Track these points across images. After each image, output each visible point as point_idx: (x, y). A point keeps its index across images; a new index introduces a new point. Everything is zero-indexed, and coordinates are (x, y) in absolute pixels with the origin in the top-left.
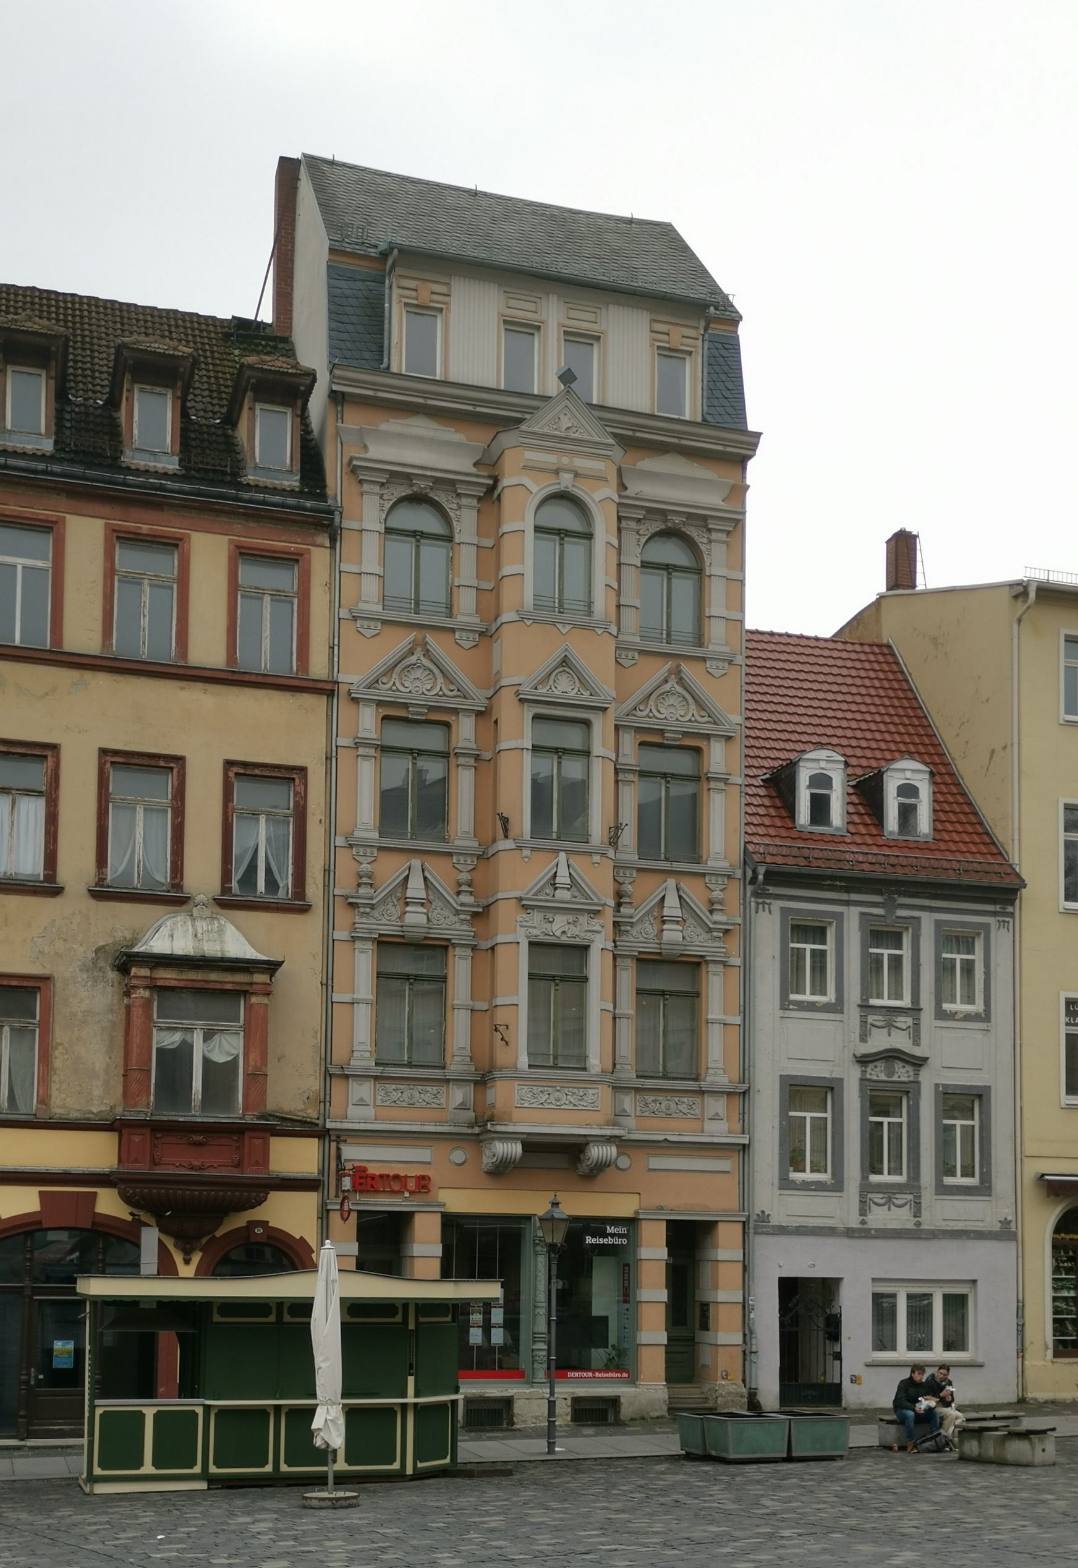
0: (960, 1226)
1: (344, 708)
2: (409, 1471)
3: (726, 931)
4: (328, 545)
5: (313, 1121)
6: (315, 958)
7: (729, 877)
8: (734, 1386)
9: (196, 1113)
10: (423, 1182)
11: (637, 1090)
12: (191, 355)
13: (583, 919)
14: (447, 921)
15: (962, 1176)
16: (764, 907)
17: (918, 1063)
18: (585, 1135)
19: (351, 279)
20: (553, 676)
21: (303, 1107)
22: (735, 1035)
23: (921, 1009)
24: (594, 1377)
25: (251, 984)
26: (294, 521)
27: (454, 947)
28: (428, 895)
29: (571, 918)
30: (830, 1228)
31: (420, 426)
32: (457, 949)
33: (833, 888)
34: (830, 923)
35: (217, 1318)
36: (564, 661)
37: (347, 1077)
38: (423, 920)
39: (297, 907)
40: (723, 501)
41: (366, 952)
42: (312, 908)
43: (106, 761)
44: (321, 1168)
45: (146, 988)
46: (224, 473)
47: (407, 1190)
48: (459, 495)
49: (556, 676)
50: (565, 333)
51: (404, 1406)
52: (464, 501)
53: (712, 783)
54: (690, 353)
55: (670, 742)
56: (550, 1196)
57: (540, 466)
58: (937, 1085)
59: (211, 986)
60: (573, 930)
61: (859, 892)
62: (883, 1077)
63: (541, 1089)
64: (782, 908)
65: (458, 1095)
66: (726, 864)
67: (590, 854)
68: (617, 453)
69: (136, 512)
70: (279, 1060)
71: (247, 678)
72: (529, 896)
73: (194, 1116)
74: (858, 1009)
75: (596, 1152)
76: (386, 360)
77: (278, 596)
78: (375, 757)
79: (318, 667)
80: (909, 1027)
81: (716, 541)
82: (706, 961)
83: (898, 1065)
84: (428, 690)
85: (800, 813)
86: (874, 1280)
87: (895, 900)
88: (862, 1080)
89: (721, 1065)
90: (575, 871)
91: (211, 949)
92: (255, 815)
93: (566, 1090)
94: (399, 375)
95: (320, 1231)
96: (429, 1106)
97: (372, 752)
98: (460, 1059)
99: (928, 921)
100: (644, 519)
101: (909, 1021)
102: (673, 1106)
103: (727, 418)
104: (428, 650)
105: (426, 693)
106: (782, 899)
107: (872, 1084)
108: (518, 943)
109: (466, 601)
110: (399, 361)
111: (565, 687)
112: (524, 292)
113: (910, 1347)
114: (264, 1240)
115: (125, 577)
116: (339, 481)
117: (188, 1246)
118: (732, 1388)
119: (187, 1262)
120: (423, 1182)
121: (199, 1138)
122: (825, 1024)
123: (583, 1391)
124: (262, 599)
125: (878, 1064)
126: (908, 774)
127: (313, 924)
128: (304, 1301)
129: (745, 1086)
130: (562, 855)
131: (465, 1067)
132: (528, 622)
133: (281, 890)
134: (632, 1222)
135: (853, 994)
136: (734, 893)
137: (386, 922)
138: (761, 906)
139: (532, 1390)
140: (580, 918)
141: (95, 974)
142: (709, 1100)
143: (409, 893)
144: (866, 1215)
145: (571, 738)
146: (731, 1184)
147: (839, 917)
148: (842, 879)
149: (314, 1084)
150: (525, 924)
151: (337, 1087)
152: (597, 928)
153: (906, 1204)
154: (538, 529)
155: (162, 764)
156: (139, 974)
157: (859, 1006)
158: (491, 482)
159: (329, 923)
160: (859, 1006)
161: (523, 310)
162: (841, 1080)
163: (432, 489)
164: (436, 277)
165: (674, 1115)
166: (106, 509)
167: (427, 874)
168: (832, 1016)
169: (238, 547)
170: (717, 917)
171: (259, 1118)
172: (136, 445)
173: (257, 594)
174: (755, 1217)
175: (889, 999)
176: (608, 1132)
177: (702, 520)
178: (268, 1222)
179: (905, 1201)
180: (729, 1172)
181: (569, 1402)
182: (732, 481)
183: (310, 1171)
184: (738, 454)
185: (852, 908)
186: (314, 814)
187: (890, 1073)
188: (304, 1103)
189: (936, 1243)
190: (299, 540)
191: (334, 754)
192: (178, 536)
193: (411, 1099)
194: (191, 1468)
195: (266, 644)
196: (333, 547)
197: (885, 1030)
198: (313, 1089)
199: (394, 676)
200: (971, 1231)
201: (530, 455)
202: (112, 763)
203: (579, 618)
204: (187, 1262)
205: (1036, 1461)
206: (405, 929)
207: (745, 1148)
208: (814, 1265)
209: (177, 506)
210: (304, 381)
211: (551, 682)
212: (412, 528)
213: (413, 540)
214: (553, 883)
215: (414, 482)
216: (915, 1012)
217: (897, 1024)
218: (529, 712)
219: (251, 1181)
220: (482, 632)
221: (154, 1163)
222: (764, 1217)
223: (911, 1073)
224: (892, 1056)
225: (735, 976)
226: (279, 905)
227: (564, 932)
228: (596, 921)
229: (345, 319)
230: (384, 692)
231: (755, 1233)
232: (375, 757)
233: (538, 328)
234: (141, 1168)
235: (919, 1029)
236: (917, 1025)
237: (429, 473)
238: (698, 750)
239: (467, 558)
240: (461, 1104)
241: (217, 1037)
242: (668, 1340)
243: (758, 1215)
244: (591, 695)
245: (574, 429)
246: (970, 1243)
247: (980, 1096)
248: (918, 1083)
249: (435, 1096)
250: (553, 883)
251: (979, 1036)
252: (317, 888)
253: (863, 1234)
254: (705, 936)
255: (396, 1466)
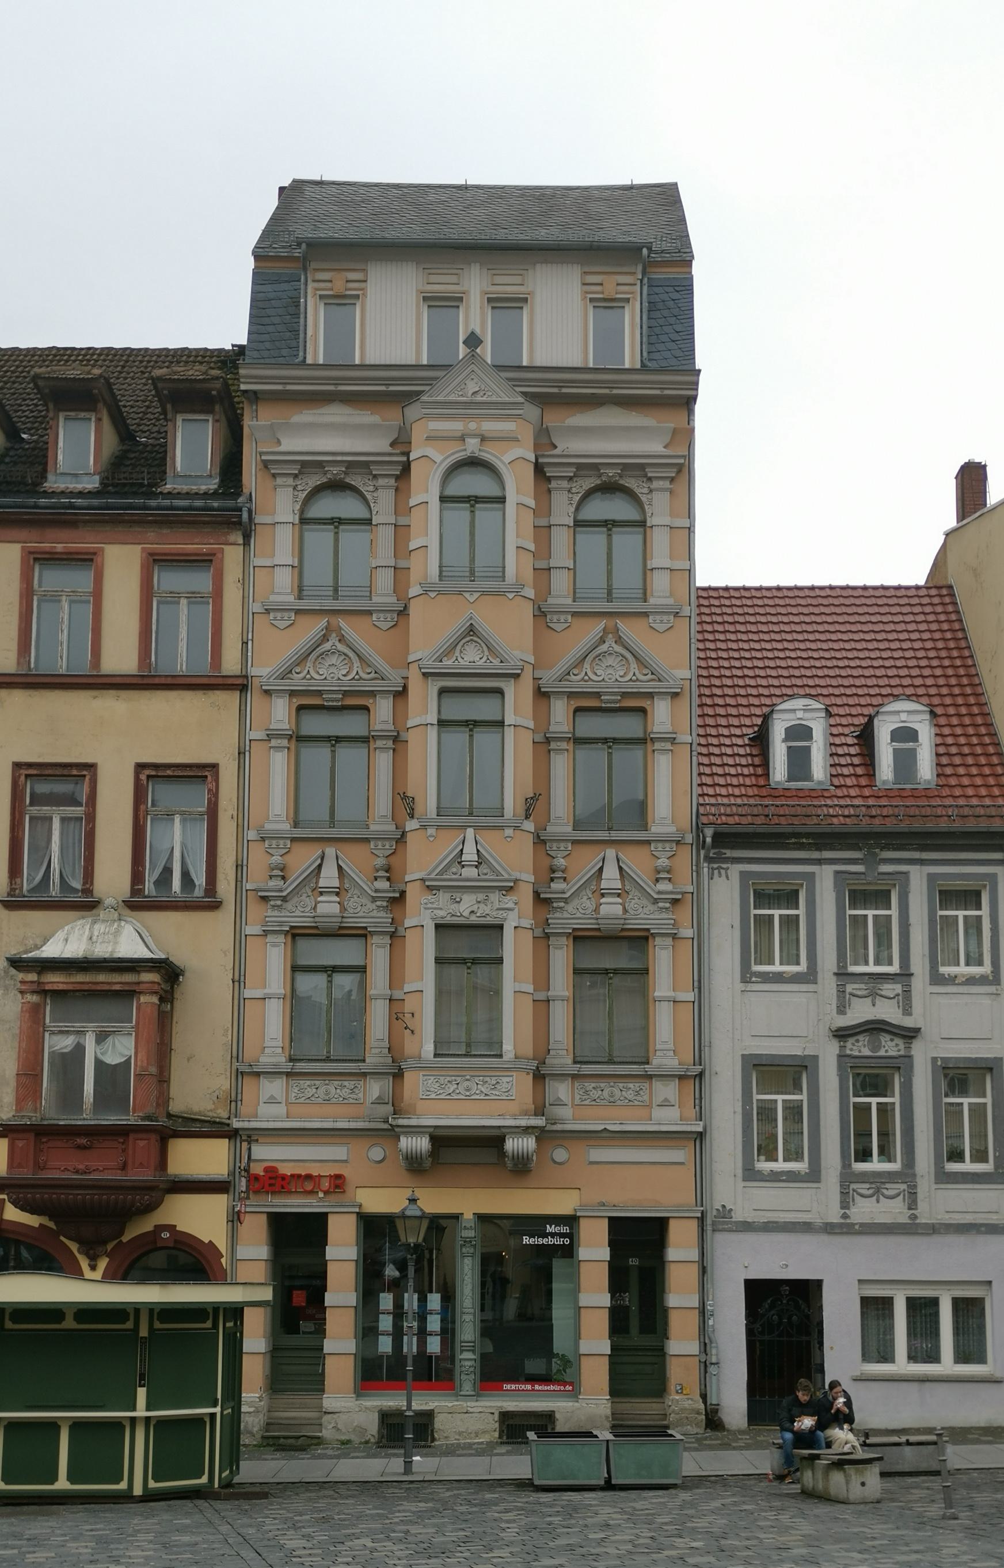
0: (968, 1219)
1: (255, 699)
2: (138, 1491)
3: (675, 902)
4: (241, 541)
5: (224, 1120)
6: (226, 955)
7: (678, 842)
8: (690, 1402)
9: (87, 1117)
10: (338, 1182)
11: (574, 1077)
12: (101, 376)
13: (495, 897)
14: (646, 910)
15: (972, 1161)
16: (720, 873)
17: (910, 1035)
18: (499, 1127)
19: (278, 282)
20: (459, 647)
21: (213, 1106)
22: (686, 1014)
23: (912, 974)
24: (533, 1390)
25: (139, 983)
26: (205, 523)
27: (372, 935)
28: (623, 885)
29: (481, 897)
30: (805, 1223)
31: (336, 414)
32: (374, 937)
33: (801, 847)
34: (985, 886)
35: (9, 1325)
36: (471, 630)
37: (258, 1074)
38: (618, 910)
39: (206, 904)
40: (665, 447)
41: (278, 946)
42: (224, 903)
43: (20, 775)
44: (232, 1168)
45: (33, 992)
46: (142, 485)
47: (322, 1191)
48: (650, 479)
49: (463, 646)
50: (489, 300)
51: (133, 1420)
52: (381, 482)
53: (656, 744)
54: (628, 300)
55: (609, 705)
56: (408, 1193)
57: (445, 435)
58: (934, 1060)
59: (99, 988)
60: (483, 909)
61: (832, 848)
62: (866, 1052)
63: (449, 1079)
64: (741, 873)
65: (375, 1088)
66: (673, 829)
67: (501, 828)
68: (532, 412)
69: (51, 533)
70: (188, 1060)
71: (157, 681)
72: (433, 876)
73: (84, 1119)
74: (834, 978)
75: (512, 1145)
76: (301, 354)
77: (194, 598)
78: (567, 750)
79: (231, 664)
80: (898, 995)
81: (657, 490)
82: (652, 934)
83: (885, 1039)
84: (621, 677)
85: (775, 769)
86: (860, 1281)
87: (875, 855)
88: (840, 1056)
89: (672, 1046)
90: (484, 848)
91: (102, 951)
92: (170, 815)
93: (477, 1079)
94: (316, 366)
95: (230, 1234)
96: (631, 1103)
97: (285, 742)
98: (377, 1051)
99: (918, 878)
100: (574, 476)
101: (898, 988)
102: (617, 1092)
103: (674, 362)
104: (620, 637)
105: (619, 679)
106: (742, 863)
107: (853, 1060)
108: (423, 926)
109: (384, 581)
110: (317, 352)
111: (471, 657)
112: (446, 266)
113: (912, 1358)
114: (171, 1245)
115: (44, 595)
116: (254, 478)
117: (92, 1252)
118: (687, 1404)
119: (93, 1268)
120: (338, 1182)
121: (83, 1141)
122: (796, 997)
123: (512, 1405)
124: (179, 603)
125: (861, 1037)
126: (903, 716)
127: (220, 923)
128: (201, 1306)
129: (699, 1068)
130: (470, 832)
131: (382, 1060)
132: (433, 595)
133: (197, 888)
134: (571, 1220)
135: (828, 961)
136: (684, 859)
137: (298, 914)
138: (716, 872)
139: (456, 1403)
140: (491, 896)
141: (7, 982)
142: (657, 1085)
143: (604, 884)
144: (849, 1209)
145: (482, 709)
146: (686, 1176)
147: (811, 877)
148: (808, 835)
149: (223, 1083)
150: (430, 905)
151: (248, 1083)
152: (510, 905)
153: (898, 1195)
154: (443, 499)
155: (75, 772)
156: (26, 980)
157: (835, 974)
158: (404, 459)
159: (240, 918)
160: (835, 974)
161: (443, 284)
162: (815, 1058)
163: (621, 477)
164: (352, 266)
165: (619, 1103)
166: (23, 533)
167: (340, 863)
168: (804, 987)
169: (151, 554)
170: (663, 886)
171: (143, 1119)
172: (60, 470)
173: (174, 598)
174: (715, 1213)
175: (781, 964)
176: (523, 1122)
177: (639, 469)
178: (175, 1226)
179: (898, 1191)
180: (682, 1163)
181: (496, 1417)
182: (672, 425)
183: (220, 1173)
184: (681, 397)
185: (824, 867)
186: (225, 810)
187: (876, 1047)
188: (214, 1103)
189: (936, 1239)
190: (212, 541)
191: (247, 748)
192: (92, 551)
193: (327, 1095)
194: (118, 1483)
195: (183, 646)
196: (246, 543)
197: (869, 1000)
198: (224, 1088)
199: (308, 664)
200: (982, 1225)
201: (435, 425)
202: (27, 776)
203: (488, 584)
204: (93, 1268)
205: (852, 1497)
206: (317, 919)
207: (701, 1136)
208: (787, 1266)
209: (208, 523)
210: (212, 386)
211: (457, 653)
212: (329, 516)
213: (605, 529)
214: (459, 859)
215: (326, 469)
216: (904, 978)
217: (883, 993)
218: (433, 687)
219: (132, 1184)
220: (401, 611)
221: (39, 1167)
222: (725, 1213)
223: (902, 1046)
224: (875, 1028)
225: (686, 949)
226: (187, 904)
227: (472, 912)
228: (508, 898)
229: (266, 321)
230: (297, 681)
231: (714, 1231)
232: (288, 749)
233: (525, 300)
234: (26, 1173)
235: (910, 996)
236: (907, 993)
237: (339, 458)
238: (643, 711)
239: (385, 536)
240: (379, 1098)
241: (110, 1040)
242: (612, 1350)
243: (717, 1210)
244: (502, 662)
245: (482, 393)
246: (981, 1239)
247: (991, 1069)
248: (910, 1057)
249: (638, 1093)
250: (459, 859)
251: (986, 1001)
252: (229, 883)
253: (845, 1230)
254: (652, 908)
255: (123, 1485)
